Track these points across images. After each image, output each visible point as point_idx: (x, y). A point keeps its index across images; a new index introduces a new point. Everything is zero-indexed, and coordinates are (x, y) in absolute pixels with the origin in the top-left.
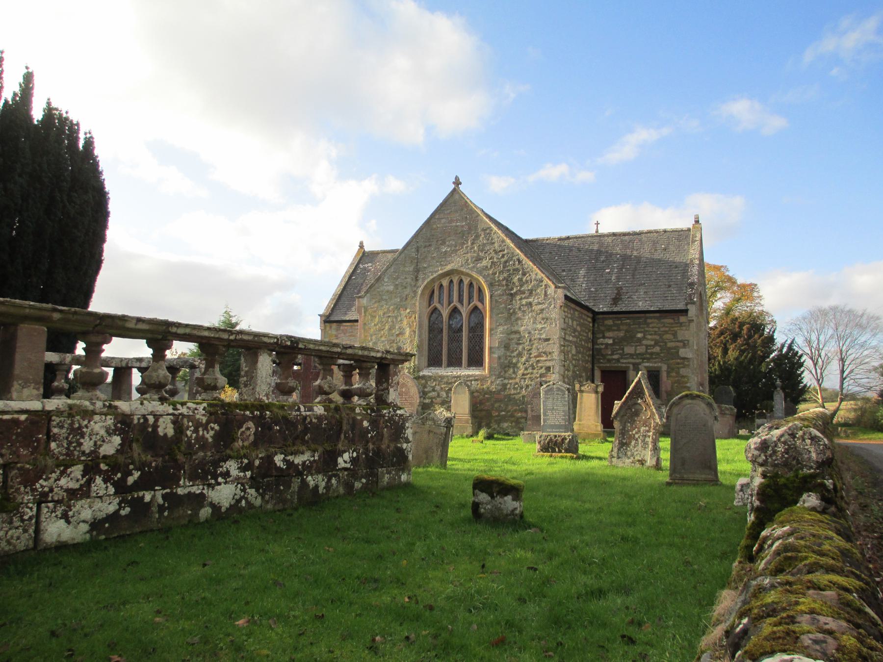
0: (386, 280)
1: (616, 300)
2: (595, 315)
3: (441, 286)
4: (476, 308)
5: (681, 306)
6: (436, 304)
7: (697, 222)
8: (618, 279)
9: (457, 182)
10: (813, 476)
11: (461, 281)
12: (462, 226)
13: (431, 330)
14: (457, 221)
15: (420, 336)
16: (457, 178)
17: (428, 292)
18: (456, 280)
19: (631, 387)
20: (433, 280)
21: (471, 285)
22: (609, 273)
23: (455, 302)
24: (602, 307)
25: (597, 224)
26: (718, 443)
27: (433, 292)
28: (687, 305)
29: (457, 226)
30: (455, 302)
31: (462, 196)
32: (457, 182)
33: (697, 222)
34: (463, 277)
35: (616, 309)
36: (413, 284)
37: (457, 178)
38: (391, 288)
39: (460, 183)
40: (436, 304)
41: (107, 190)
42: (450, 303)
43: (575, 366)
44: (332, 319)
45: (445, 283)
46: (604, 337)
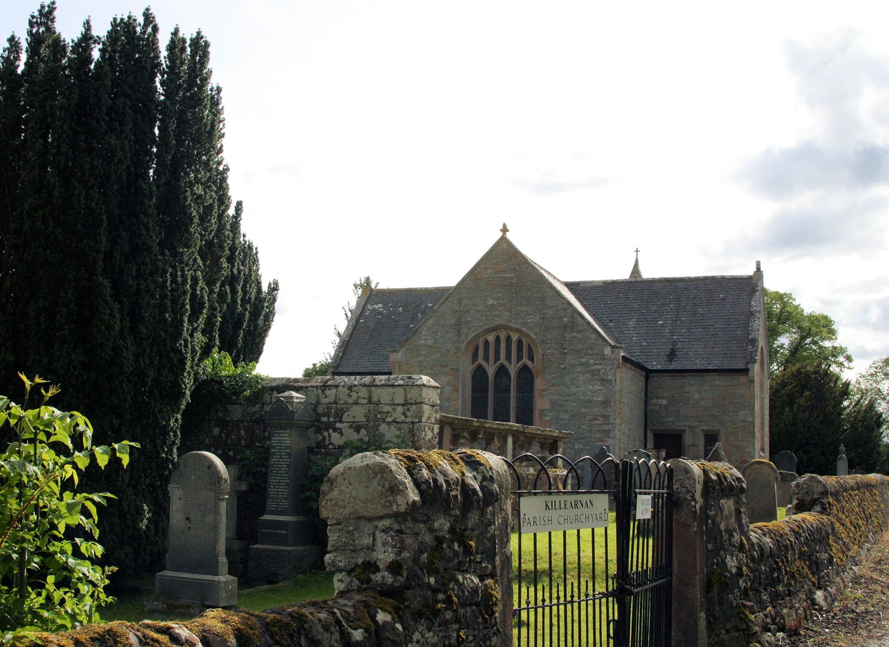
0: (424, 333)
1: (672, 355)
2: (648, 374)
3: (486, 343)
4: (525, 368)
5: (740, 365)
6: (481, 361)
7: (758, 269)
8: (672, 333)
9: (505, 230)
10: (818, 499)
11: (509, 339)
12: (511, 278)
13: (475, 389)
14: (505, 272)
15: (463, 396)
16: (504, 225)
17: (471, 349)
18: (503, 335)
19: (282, 548)
20: (477, 336)
21: (520, 342)
22: (662, 325)
23: (503, 360)
24: (655, 365)
25: (637, 251)
26: (778, 508)
27: (477, 348)
28: (747, 364)
29: (505, 278)
30: (503, 360)
31: (510, 245)
32: (505, 230)
33: (758, 269)
34: (512, 334)
35: (671, 367)
36: (455, 339)
37: (504, 225)
38: (430, 342)
39: (508, 231)
40: (481, 361)
41: (266, 276)
42: (496, 361)
43: (629, 430)
44: (341, 370)
45: (491, 338)
46: (658, 398)
